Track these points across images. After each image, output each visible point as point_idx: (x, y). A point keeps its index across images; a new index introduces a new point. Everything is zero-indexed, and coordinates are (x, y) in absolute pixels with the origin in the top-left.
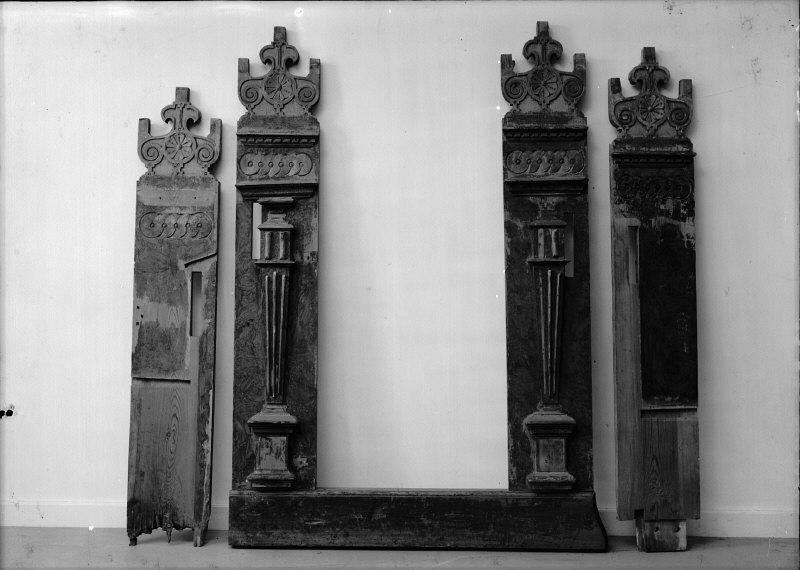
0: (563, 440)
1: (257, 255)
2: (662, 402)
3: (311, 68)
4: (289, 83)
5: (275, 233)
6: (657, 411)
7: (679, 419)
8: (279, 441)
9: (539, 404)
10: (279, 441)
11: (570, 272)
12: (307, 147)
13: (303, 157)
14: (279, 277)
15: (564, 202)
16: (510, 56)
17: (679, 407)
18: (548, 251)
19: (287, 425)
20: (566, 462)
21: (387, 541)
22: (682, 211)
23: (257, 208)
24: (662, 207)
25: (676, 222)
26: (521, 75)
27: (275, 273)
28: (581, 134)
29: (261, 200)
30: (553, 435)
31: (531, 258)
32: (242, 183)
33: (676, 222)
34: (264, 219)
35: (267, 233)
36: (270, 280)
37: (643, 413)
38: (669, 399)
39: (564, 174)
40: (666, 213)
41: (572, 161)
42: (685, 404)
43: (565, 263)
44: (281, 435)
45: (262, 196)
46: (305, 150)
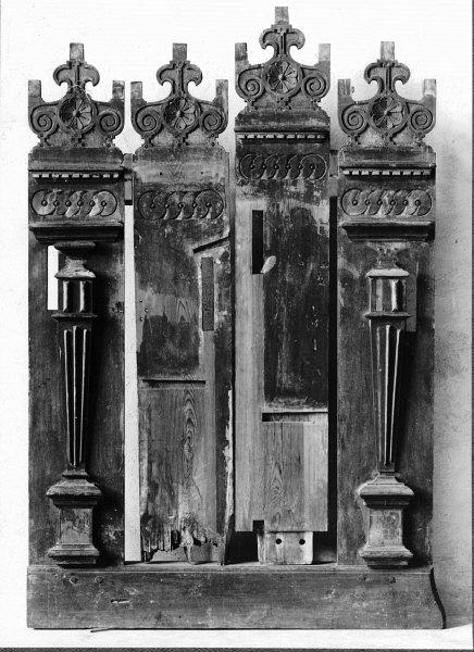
0: (400, 512)
1: (53, 304)
2: (287, 404)
3: (114, 92)
4: (88, 109)
5: (75, 282)
6: (282, 415)
7: (306, 423)
8: (85, 513)
9: (374, 473)
10: (85, 513)
11: (412, 325)
12: (109, 183)
13: (107, 196)
14: (79, 332)
15: (406, 250)
16: (348, 81)
17: (305, 410)
18: (387, 307)
19: (91, 497)
20: (404, 536)
21: (188, 623)
22: (315, 193)
23: (53, 253)
24: (293, 189)
25: (307, 206)
26: (361, 104)
27: (75, 328)
28: (427, 172)
29: (60, 244)
30: (389, 507)
31: (369, 312)
32: (34, 225)
33: (307, 206)
34: (62, 265)
35: (65, 284)
36: (70, 335)
37: (266, 417)
38: (296, 401)
39: (408, 216)
40: (297, 196)
41: (418, 203)
42: (314, 406)
43: (405, 318)
44: (84, 507)
45: (58, 240)
46: (107, 187)
